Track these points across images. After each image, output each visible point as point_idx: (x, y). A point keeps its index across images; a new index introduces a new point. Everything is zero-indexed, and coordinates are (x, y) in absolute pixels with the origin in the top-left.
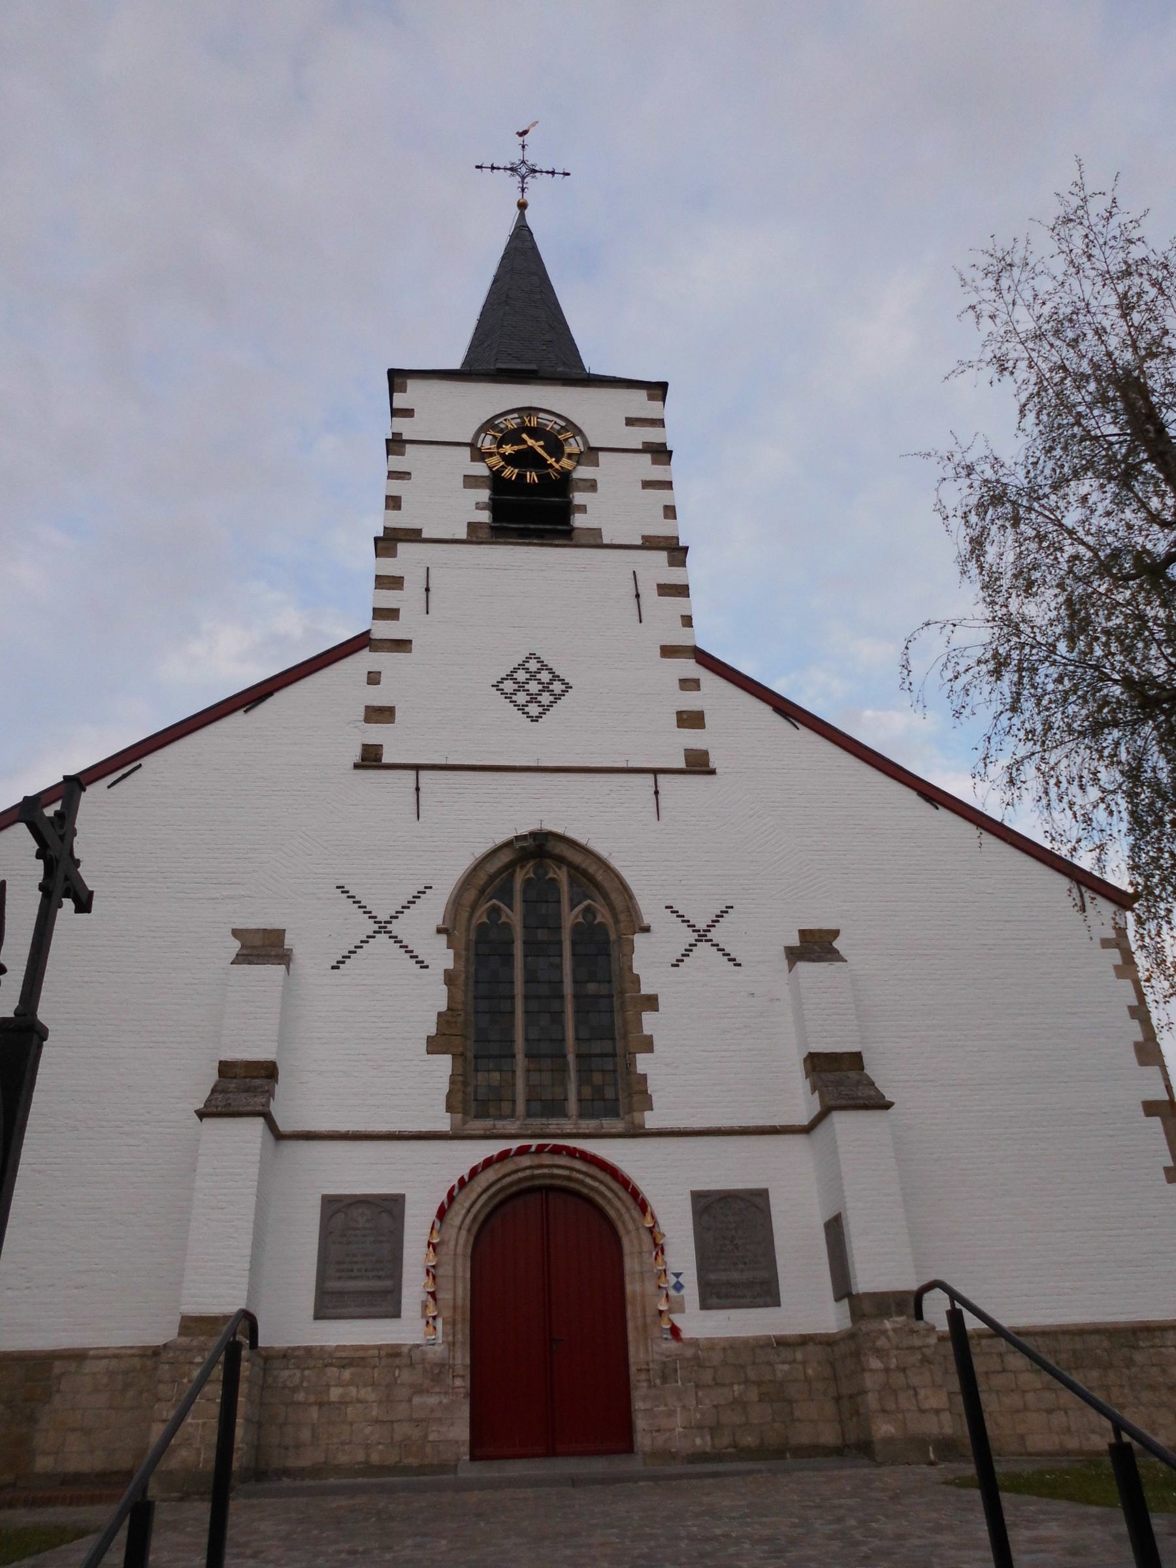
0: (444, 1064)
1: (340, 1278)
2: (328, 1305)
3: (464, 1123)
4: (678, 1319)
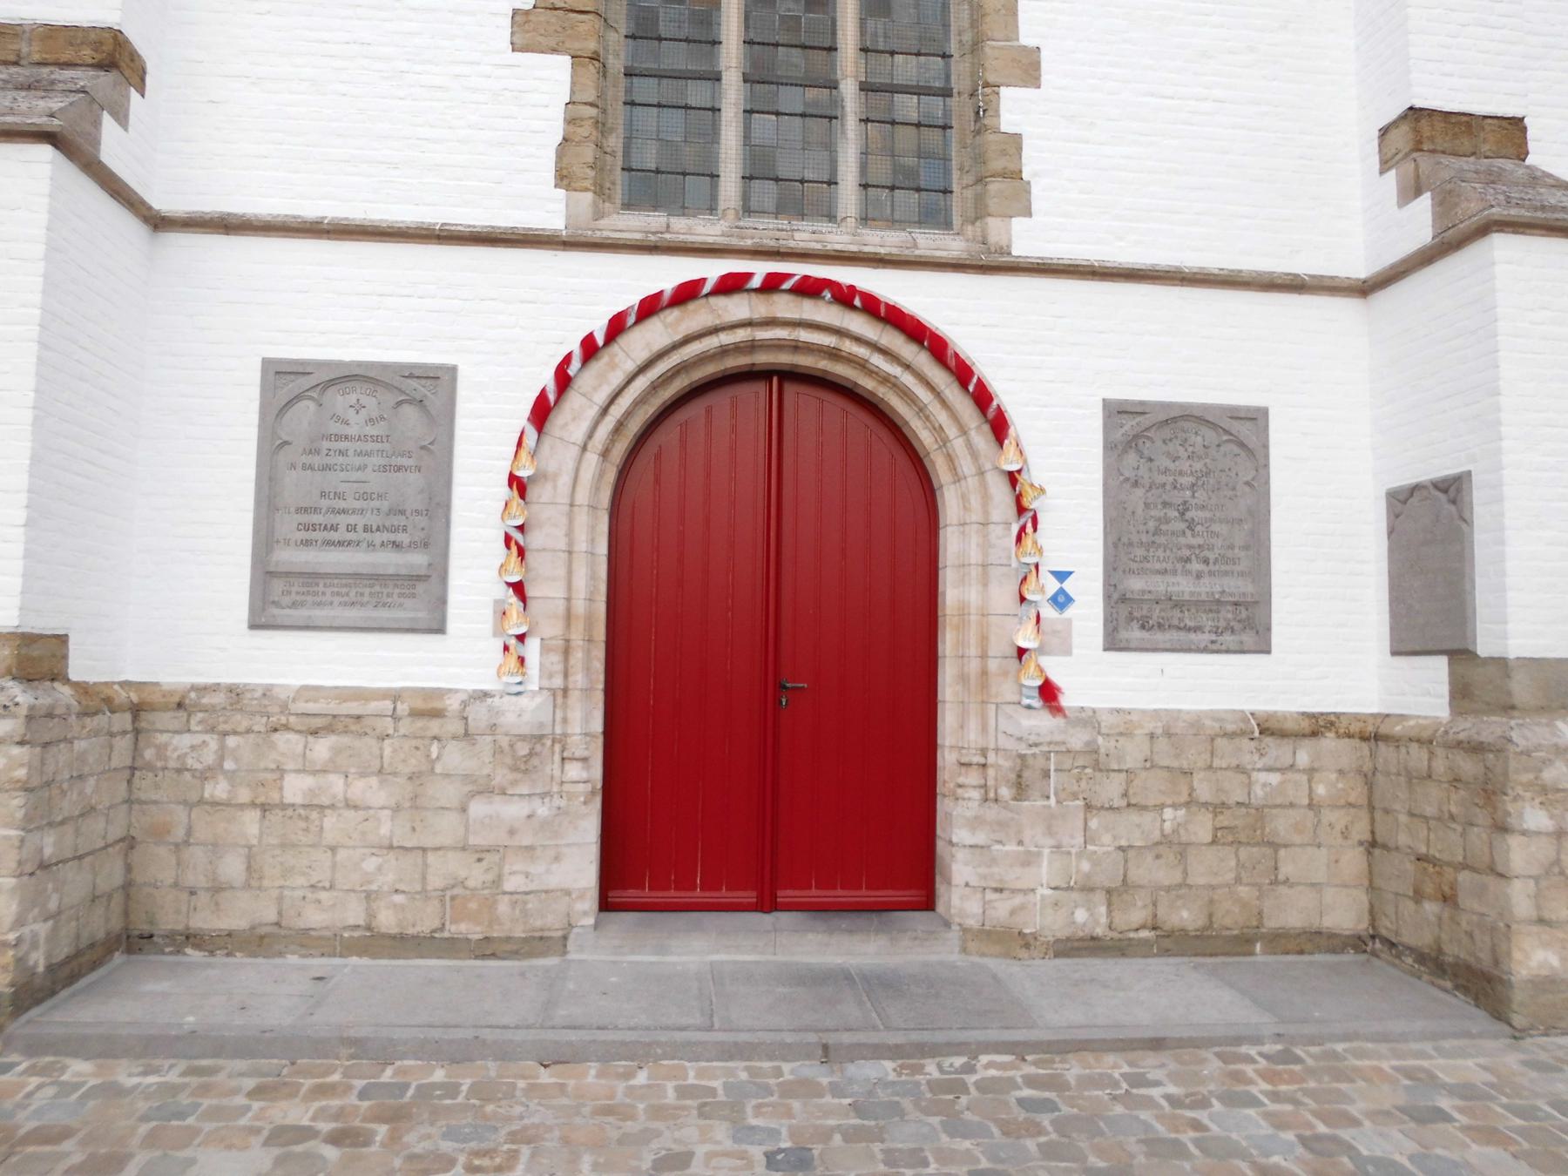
0: (551, 79)
1: (307, 543)
2: (278, 598)
3: (598, 215)
4: (1057, 669)
